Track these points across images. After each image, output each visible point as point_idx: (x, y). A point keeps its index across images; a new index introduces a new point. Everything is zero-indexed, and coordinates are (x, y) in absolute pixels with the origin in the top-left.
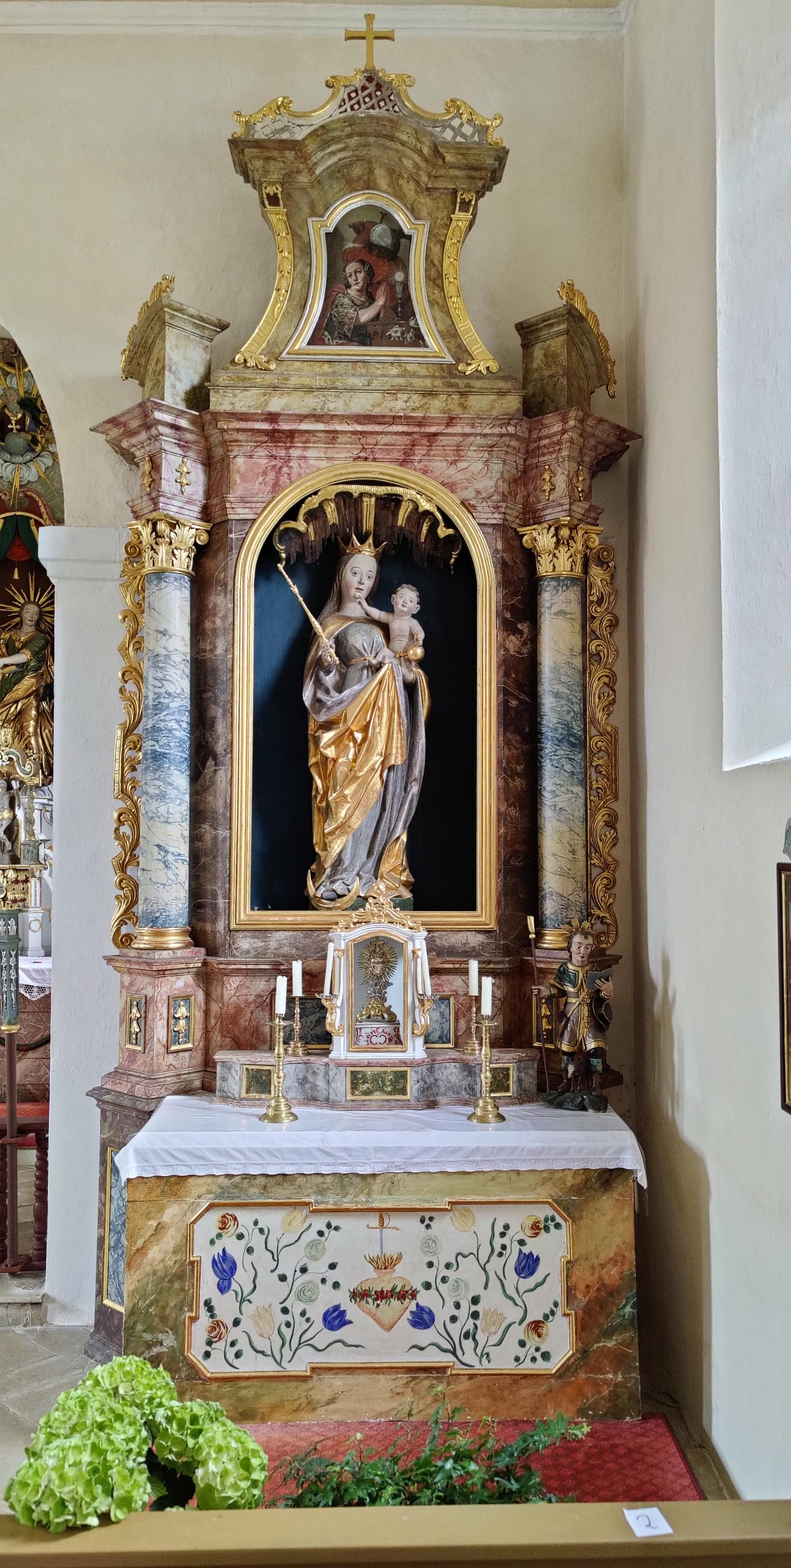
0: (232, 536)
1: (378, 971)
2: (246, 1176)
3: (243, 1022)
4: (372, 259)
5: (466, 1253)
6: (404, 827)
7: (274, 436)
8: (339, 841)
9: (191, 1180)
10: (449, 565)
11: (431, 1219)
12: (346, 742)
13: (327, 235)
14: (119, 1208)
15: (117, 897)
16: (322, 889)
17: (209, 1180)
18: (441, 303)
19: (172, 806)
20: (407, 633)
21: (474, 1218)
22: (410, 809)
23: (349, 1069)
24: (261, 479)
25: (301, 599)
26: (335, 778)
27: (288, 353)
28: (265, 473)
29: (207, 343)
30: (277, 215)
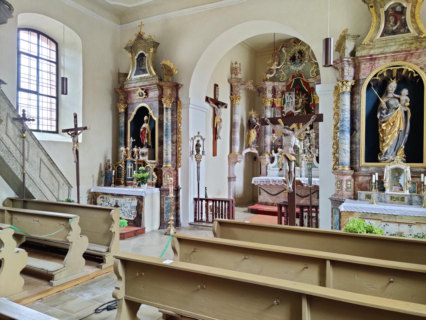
0: (361, 82)
1: (397, 175)
2: (367, 213)
3: (363, 186)
4: (396, 15)
5: (420, 233)
6: (404, 144)
7: (371, 59)
8: (386, 148)
9: (355, 212)
10: (417, 82)
11: (411, 225)
12: (389, 126)
13: (385, 11)
14: (336, 221)
15: (333, 160)
16: (382, 158)
17: (359, 213)
18: (414, 21)
19: (346, 141)
20: (405, 100)
21: (422, 226)
22: (405, 140)
23: (390, 195)
24: (368, 69)
25: (377, 95)
26: (386, 134)
27: (375, 40)
28: (369, 68)
29: (355, 41)
30: (372, 10)
